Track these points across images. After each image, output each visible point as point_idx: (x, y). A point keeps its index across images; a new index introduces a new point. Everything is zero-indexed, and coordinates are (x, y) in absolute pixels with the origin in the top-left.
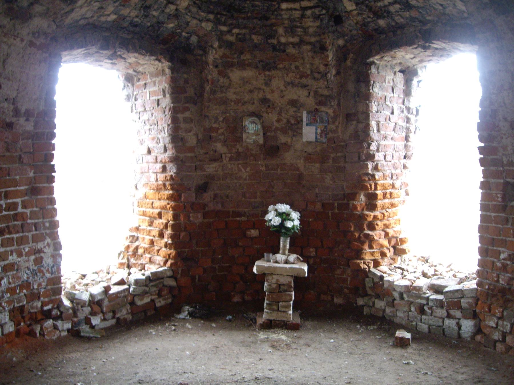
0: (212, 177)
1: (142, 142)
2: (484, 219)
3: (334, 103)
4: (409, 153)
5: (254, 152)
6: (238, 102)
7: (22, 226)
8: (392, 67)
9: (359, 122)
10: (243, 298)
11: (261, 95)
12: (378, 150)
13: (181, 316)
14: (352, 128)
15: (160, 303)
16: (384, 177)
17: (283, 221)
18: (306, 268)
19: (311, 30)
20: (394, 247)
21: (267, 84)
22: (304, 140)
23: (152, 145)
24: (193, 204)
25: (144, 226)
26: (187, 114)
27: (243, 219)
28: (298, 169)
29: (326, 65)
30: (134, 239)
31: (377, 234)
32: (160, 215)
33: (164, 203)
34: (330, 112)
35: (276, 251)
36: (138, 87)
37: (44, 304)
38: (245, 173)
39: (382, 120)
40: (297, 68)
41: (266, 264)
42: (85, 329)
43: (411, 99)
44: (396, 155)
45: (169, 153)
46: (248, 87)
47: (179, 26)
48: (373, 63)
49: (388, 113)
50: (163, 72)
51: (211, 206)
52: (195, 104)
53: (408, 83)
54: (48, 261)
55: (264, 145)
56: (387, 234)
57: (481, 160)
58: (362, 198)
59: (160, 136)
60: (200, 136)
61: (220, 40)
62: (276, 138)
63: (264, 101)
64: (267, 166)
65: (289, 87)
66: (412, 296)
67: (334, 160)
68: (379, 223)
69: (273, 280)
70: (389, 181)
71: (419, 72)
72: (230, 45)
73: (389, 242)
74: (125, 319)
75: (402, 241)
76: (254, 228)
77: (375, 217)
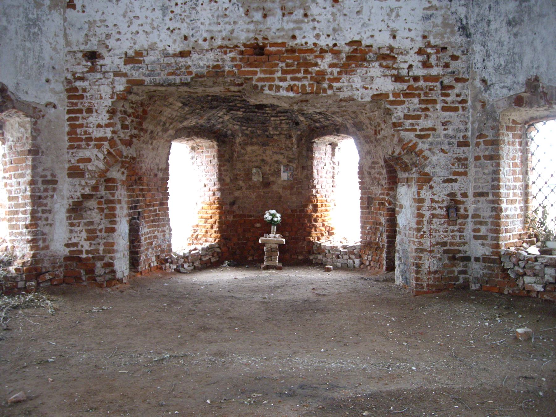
0: (237, 198)
1: (200, 181)
2: (362, 213)
3: (296, 161)
4: (334, 185)
5: (258, 185)
6: (250, 161)
7: (159, 219)
8: (325, 143)
9: (308, 170)
10: (253, 258)
11: (261, 158)
12: (318, 184)
13: (224, 265)
14: (305, 172)
15: (213, 260)
17: (273, 217)
18: (284, 240)
19: (284, 129)
20: (328, 232)
21: (264, 153)
22: (282, 179)
23: (207, 182)
24: (228, 211)
25: (202, 223)
26: (225, 167)
27: (253, 218)
28: (279, 193)
29: (292, 144)
30: (196, 231)
31: (318, 224)
32: (211, 217)
33: (214, 211)
34: (294, 165)
35: (269, 232)
36: (198, 153)
37: (166, 256)
38: (253, 196)
39: (320, 169)
40: (278, 145)
41: (265, 239)
42: (182, 270)
43: (335, 157)
44: (328, 186)
45: (217, 186)
46: (255, 154)
47: (223, 127)
48: (314, 142)
49: (322, 165)
50: (213, 147)
51: (238, 212)
52: (229, 162)
53: (333, 150)
54: (167, 236)
55: (262, 182)
56: (323, 225)
57: (360, 187)
58: (311, 207)
59: (212, 178)
60: (232, 178)
61: (242, 133)
62: (268, 178)
63: (263, 160)
64: (264, 192)
65: (275, 154)
66: (334, 251)
67: (297, 189)
68: (319, 219)
70: (324, 198)
71: (339, 144)
72: (247, 135)
73: (326, 228)
74: (198, 267)
75: (332, 229)
76: (258, 223)
77: (317, 216)
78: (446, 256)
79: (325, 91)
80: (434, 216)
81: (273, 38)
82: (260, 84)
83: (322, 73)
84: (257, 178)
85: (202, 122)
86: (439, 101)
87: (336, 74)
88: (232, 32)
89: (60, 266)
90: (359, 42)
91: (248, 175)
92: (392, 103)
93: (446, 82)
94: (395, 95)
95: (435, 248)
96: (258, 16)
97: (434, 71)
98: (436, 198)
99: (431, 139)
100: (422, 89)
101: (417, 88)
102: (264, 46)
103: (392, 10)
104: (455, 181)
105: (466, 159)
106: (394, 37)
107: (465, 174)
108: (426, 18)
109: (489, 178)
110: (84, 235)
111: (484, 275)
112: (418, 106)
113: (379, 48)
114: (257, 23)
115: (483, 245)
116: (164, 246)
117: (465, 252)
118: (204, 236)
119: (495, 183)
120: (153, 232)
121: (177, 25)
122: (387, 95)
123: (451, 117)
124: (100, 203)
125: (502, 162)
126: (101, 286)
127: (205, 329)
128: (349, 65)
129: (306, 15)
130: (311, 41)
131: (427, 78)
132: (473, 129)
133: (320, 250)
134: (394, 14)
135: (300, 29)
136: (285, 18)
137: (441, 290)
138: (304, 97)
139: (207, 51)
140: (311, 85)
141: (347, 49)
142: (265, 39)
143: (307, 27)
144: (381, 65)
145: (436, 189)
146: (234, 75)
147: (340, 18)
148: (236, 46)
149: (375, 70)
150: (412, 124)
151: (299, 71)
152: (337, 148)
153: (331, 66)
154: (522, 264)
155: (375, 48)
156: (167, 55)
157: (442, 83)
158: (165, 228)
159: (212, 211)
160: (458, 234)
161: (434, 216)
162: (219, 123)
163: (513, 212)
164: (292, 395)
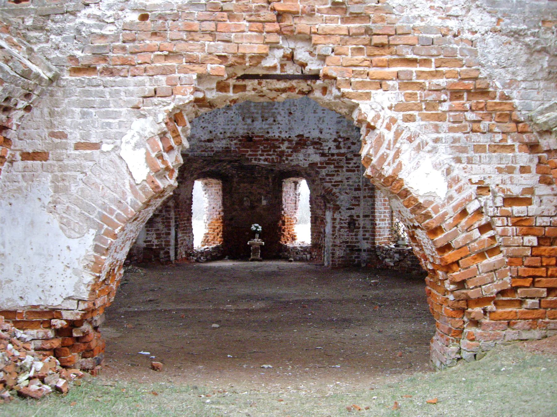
15: (219, 255)
16: (288, 215)
30: (207, 237)
31: (286, 233)
32: (217, 228)
35: (254, 238)
36: (209, 187)
39: (287, 198)
42: (200, 261)
45: (221, 209)
50: (219, 184)
53: (296, 186)
54: (191, 239)
58: (281, 222)
63: (250, 193)
69: (254, 246)
72: (240, 177)
78: (348, 249)
79: (284, 161)
80: (341, 227)
81: (257, 133)
82: (250, 157)
83: (282, 152)
84: (247, 204)
85: (213, 168)
86: (345, 167)
87: (290, 152)
88: (235, 129)
89: (141, 253)
90: (302, 136)
91: (241, 202)
92: (319, 168)
93: (349, 156)
94: (321, 163)
95: (342, 244)
96: (249, 121)
97: (342, 151)
98: (342, 218)
99: (340, 187)
100: (335, 160)
101: (333, 160)
102: (253, 137)
103: (320, 118)
104: (353, 209)
105: (359, 197)
106: (321, 133)
107: (358, 205)
108: (338, 122)
109: (370, 207)
110: (155, 236)
111: (368, 259)
112: (333, 169)
113: (313, 139)
114: (249, 125)
115: (367, 242)
116: (190, 245)
117: (358, 247)
118: (212, 240)
119: (373, 210)
120: (183, 236)
121: (206, 125)
122: (317, 164)
123: (351, 175)
124: (163, 219)
125: (376, 199)
126: (162, 264)
127: (221, 281)
128: (297, 148)
129: (274, 121)
130: (277, 135)
131: (338, 155)
132: (363, 181)
133: (286, 249)
134: (321, 120)
135: (272, 128)
136: (264, 123)
137: (346, 267)
138: (273, 164)
139: (222, 139)
140: (277, 158)
141: (296, 139)
142: (253, 133)
143: (275, 127)
144: (314, 148)
145: (343, 213)
146: (236, 152)
147: (293, 123)
148: (238, 137)
149: (311, 150)
150: (330, 179)
151: (270, 151)
152: (298, 185)
153: (288, 148)
154: (384, 252)
155: (311, 138)
156: (201, 141)
157: (346, 157)
158: (190, 235)
159: (218, 224)
160: (354, 237)
161: (341, 227)
162: (224, 169)
163: (384, 226)
164: (263, 299)
